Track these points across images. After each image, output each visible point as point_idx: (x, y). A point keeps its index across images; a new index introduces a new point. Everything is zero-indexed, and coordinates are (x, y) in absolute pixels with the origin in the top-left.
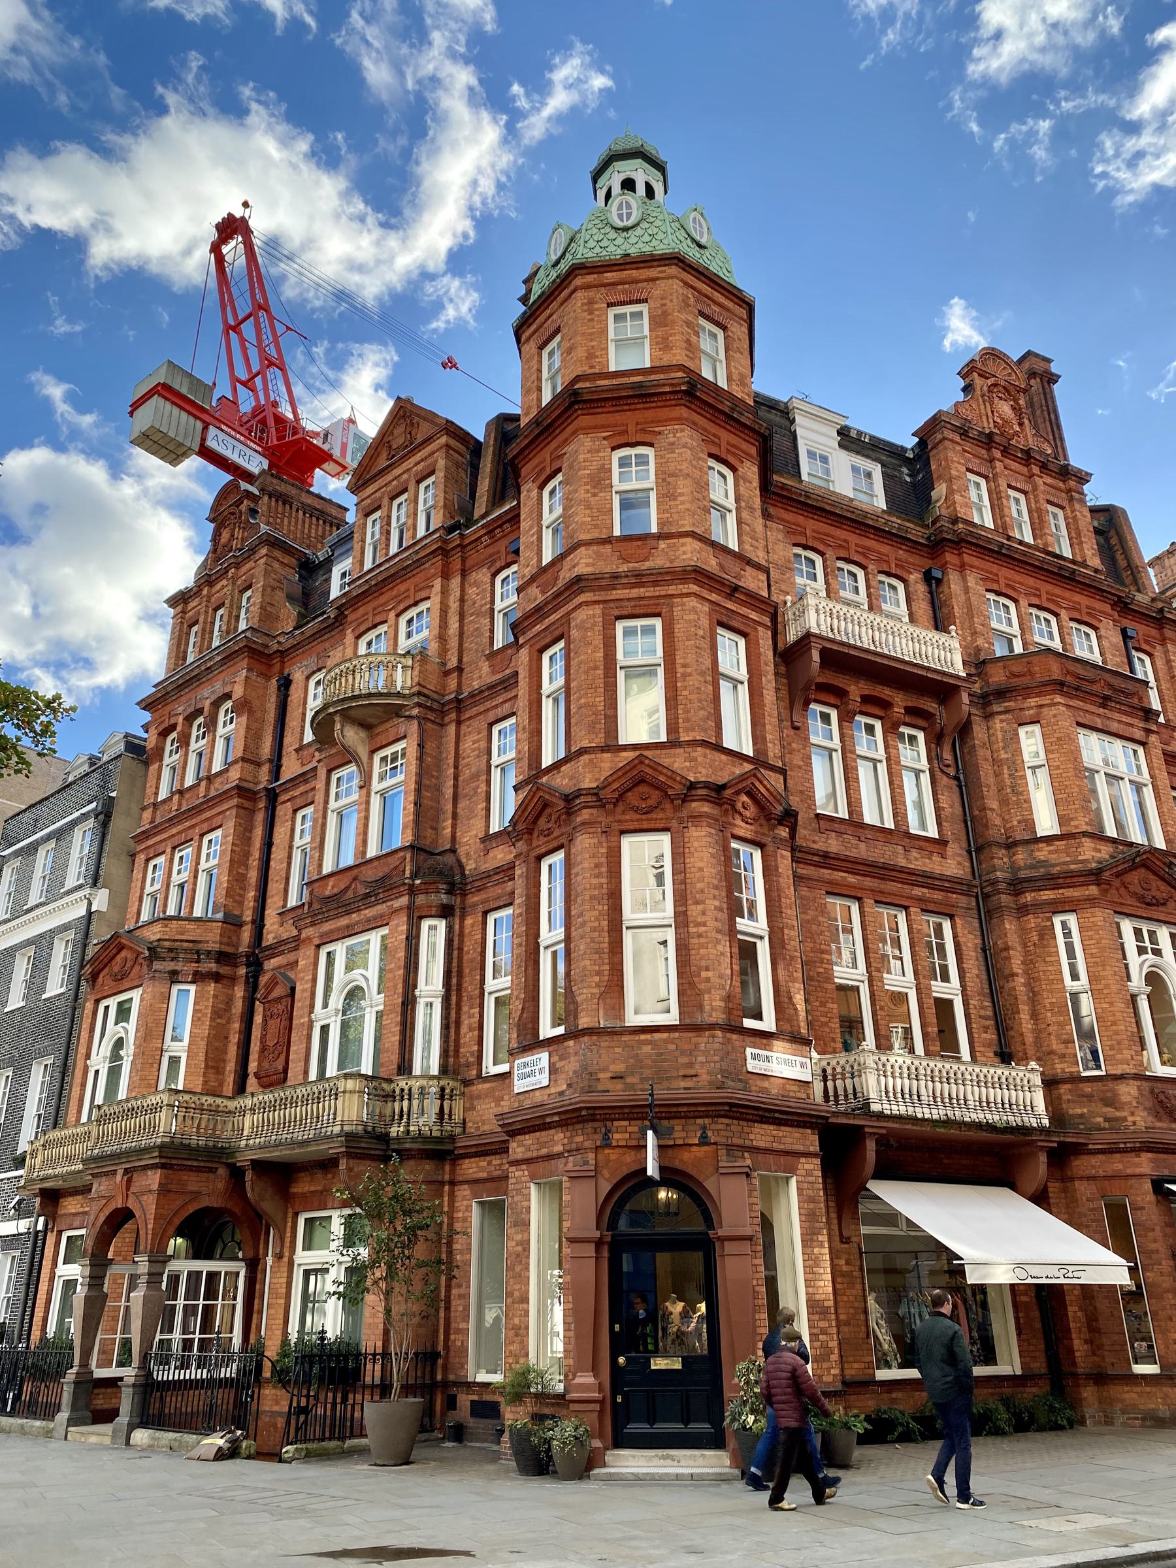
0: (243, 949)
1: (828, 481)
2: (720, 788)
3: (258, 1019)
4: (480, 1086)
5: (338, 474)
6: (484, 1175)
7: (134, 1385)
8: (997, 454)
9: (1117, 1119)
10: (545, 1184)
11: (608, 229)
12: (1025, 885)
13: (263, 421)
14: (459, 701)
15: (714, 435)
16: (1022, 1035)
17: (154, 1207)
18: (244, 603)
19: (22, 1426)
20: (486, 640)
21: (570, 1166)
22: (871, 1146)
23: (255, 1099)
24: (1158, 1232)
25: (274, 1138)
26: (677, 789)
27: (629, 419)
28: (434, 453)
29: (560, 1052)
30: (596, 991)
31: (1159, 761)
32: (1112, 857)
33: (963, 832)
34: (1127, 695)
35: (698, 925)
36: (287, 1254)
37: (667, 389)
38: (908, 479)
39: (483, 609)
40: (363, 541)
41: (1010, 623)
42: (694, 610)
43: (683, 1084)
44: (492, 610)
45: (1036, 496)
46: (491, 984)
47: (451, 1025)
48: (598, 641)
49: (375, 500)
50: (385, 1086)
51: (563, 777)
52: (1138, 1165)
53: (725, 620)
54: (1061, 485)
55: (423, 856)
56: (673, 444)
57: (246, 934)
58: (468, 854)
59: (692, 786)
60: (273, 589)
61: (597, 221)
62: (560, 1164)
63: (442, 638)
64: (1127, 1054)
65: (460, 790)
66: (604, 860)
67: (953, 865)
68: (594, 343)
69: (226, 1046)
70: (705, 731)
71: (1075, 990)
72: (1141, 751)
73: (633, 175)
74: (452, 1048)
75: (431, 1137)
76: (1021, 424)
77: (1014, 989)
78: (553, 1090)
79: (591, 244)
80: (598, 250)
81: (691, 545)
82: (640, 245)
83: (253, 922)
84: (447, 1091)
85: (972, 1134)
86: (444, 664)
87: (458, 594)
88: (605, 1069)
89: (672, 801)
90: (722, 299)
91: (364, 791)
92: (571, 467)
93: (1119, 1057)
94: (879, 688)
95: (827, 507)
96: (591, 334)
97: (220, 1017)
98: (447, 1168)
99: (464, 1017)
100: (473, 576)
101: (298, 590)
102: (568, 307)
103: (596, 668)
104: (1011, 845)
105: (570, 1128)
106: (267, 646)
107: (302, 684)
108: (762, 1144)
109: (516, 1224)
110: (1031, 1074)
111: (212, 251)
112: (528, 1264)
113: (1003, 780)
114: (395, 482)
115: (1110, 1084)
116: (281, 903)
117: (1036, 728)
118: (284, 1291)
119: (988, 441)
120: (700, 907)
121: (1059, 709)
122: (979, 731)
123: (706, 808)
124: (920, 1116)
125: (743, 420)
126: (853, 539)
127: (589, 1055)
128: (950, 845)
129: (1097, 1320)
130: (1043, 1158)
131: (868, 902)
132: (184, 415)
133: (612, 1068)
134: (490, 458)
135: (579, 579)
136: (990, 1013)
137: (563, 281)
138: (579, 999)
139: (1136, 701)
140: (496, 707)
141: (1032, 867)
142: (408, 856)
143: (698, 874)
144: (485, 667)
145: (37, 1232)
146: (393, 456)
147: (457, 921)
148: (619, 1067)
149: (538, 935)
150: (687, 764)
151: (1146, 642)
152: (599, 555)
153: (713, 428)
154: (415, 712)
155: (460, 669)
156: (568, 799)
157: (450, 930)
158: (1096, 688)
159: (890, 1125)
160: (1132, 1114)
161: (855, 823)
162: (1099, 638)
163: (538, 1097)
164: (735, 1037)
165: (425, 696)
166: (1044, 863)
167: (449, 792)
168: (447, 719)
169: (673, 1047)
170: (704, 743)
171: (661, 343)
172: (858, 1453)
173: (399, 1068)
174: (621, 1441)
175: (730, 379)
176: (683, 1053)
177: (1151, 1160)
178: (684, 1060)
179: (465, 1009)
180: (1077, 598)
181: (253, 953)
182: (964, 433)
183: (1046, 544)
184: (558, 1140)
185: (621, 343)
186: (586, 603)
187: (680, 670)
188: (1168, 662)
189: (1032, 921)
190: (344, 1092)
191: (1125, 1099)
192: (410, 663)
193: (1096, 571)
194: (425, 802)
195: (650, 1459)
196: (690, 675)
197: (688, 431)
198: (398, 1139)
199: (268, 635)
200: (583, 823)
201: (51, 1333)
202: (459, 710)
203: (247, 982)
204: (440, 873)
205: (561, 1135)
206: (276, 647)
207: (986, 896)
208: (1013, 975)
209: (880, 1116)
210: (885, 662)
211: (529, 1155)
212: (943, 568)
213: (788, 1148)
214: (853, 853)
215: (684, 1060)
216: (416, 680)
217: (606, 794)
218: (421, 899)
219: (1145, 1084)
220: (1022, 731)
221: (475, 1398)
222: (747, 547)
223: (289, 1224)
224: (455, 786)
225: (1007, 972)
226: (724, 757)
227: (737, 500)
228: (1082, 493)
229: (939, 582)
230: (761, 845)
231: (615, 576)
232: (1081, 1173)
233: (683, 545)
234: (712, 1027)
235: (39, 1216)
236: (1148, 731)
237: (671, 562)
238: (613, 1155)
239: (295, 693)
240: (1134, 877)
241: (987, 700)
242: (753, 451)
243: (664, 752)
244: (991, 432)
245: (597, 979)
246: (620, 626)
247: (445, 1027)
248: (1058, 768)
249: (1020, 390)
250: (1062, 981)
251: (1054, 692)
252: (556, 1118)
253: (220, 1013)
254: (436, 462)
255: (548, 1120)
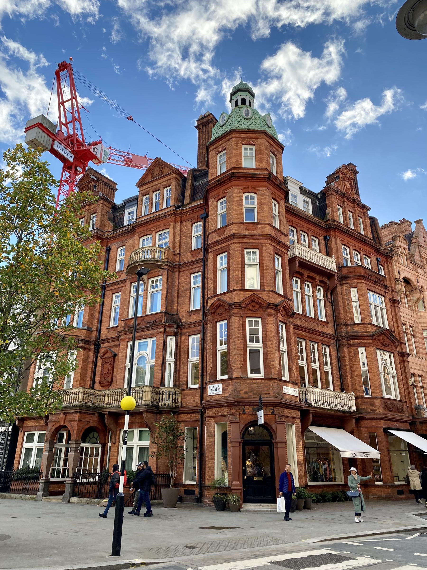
0: (93, 339)
1: (296, 204)
2: (277, 306)
3: (99, 364)
4: (188, 391)
5: (98, 163)
6: (189, 420)
7: (71, 483)
8: (346, 200)
9: (374, 410)
10: (220, 424)
11: (241, 118)
12: (351, 338)
13: (72, 141)
14: (180, 265)
15: (274, 192)
16: (348, 383)
17: (77, 426)
18: (92, 218)
19: (21, 497)
20: (189, 246)
21: (230, 419)
22: (311, 416)
23: (109, 392)
24: (384, 444)
25: (117, 405)
26: (264, 305)
27: (250, 184)
28: (170, 179)
29: (226, 384)
30: (239, 366)
31: (388, 302)
32: (376, 331)
33: (333, 320)
34: (381, 281)
35: (270, 348)
36: (117, 442)
37: (262, 176)
38: (318, 204)
39: (189, 235)
40: (142, 205)
41: (347, 255)
42: (269, 248)
43: (266, 396)
44: (192, 236)
45: (355, 214)
46: (191, 359)
47: (177, 371)
48: (239, 255)
49: (147, 191)
50: (157, 390)
51: (227, 297)
52: (380, 424)
53: (277, 252)
54: (362, 211)
55: (168, 315)
56: (263, 194)
57: (94, 334)
58: (182, 316)
59: (269, 304)
60: (104, 215)
61: (237, 114)
62: (226, 418)
63: (174, 243)
64: (378, 391)
65: (179, 294)
66: (241, 325)
67: (330, 330)
68: (238, 157)
69: (86, 372)
70: (272, 287)
71: (364, 371)
72: (383, 298)
73: (245, 97)
74: (178, 379)
75: (172, 407)
76: (352, 190)
77: (346, 369)
78: (223, 395)
79: (236, 122)
80: (238, 125)
81: (268, 227)
82: (252, 125)
83: (97, 330)
84: (177, 392)
85: (337, 413)
86: (174, 252)
87: (179, 229)
88: (242, 390)
89: (263, 309)
90: (276, 146)
91: (146, 291)
92: (230, 197)
93: (376, 392)
94: (312, 273)
95: (299, 214)
96: (237, 154)
97: (85, 362)
98: (176, 417)
99: (181, 369)
100: (185, 223)
101: (112, 216)
102: (229, 143)
103: (239, 264)
104: (347, 325)
105: (230, 407)
106: (103, 236)
107: (115, 250)
108: (287, 415)
109: (209, 436)
110: (352, 396)
111: (56, 73)
112: (214, 448)
113: (345, 305)
114: (155, 186)
115: (373, 400)
116: (108, 325)
117: (356, 289)
118: (116, 454)
119: (343, 195)
120: (271, 342)
121: (363, 284)
122: (339, 289)
123: (273, 311)
124: (324, 407)
125: (282, 187)
126: (305, 225)
127: (237, 386)
128: (329, 324)
129: (366, 469)
130: (354, 421)
131: (308, 341)
132: (46, 136)
133: (244, 390)
134: (190, 183)
135: (234, 234)
136: (339, 376)
137: (227, 134)
138: (233, 368)
139: (383, 282)
140: (193, 268)
141: (353, 332)
142: (164, 315)
143: (270, 332)
144: (189, 255)
145: (9, 432)
146: (154, 177)
147: (179, 338)
148: (247, 390)
149: (216, 347)
150: (267, 297)
151: (383, 262)
152: (240, 227)
153: (274, 190)
154: (166, 267)
155: (180, 254)
156: (230, 305)
157: (177, 340)
158: (372, 278)
159: (317, 410)
160: (379, 409)
161: (304, 316)
162: (371, 261)
163: (218, 397)
164: (280, 382)
165: (169, 262)
166: (356, 332)
167: (176, 295)
168: (175, 270)
169: (263, 385)
170: (272, 291)
171: (259, 160)
172: (313, 505)
173: (161, 384)
174: (246, 501)
175: (277, 173)
176: (266, 387)
177: (383, 423)
178: (266, 389)
179: (182, 366)
180: (366, 248)
181: (97, 341)
182: (337, 192)
183: (358, 230)
184: (226, 411)
185: (246, 158)
186: (236, 243)
187: (265, 267)
188: (388, 269)
189: (352, 349)
190: (146, 391)
191: (377, 404)
192: (164, 251)
193: (371, 239)
194: (168, 297)
195: (256, 506)
196: (268, 269)
197: (267, 190)
198: (162, 407)
199: (102, 231)
200: (235, 313)
201: (21, 466)
202: (179, 268)
203: (94, 351)
204: (174, 322)
205: (227, 410)
206: (106, 236)
207: (339, 340)
208: (346, 365)
209: (314, 407)
210: (316, 266)
211: (214, 415)
212: (330, 236)
213: (293, 416)
214: (304, 325)
215: (266, 389)
216: (166, 257)
217: (243, 305)
218: (168, 330)
219: (382, 400)
220: (352, 290)
221: (186, 489)
222: (282, 228)
223: (118, 433)
224: (178, 293)
225: (344, 364)
226: (277, 296)
227: (279, 213)
228: (368, 214)
229: (328, 240)
230: (285, 324)
231: (245, 235)
232: (363, 426)
233: (266, 227)
234: (275, 379)
235: (10, 426)
236: (386, 292)
237: (262, 232)
238: (244, 416)
239: (112, 253)
240: (381, 337)
241: (343, 279)
242: (283, 197)
243: (260, 293)
244: (345, 193)
245: (239, 362)
246: (246, 251)
247: (175, 372)
248: (362, 303)
249: (352, 179)
250: (360, 368)
251: (362, 279)
252: (226, 404)
253: (85, 360)
254: (171, 182)
255: (223, 405)
